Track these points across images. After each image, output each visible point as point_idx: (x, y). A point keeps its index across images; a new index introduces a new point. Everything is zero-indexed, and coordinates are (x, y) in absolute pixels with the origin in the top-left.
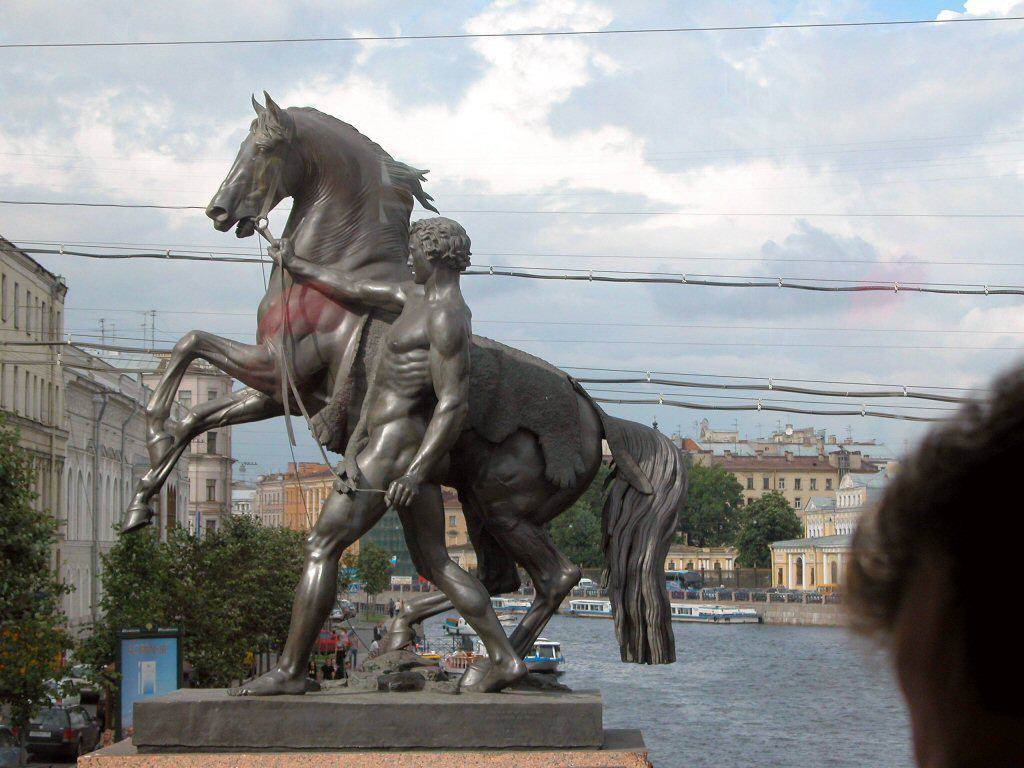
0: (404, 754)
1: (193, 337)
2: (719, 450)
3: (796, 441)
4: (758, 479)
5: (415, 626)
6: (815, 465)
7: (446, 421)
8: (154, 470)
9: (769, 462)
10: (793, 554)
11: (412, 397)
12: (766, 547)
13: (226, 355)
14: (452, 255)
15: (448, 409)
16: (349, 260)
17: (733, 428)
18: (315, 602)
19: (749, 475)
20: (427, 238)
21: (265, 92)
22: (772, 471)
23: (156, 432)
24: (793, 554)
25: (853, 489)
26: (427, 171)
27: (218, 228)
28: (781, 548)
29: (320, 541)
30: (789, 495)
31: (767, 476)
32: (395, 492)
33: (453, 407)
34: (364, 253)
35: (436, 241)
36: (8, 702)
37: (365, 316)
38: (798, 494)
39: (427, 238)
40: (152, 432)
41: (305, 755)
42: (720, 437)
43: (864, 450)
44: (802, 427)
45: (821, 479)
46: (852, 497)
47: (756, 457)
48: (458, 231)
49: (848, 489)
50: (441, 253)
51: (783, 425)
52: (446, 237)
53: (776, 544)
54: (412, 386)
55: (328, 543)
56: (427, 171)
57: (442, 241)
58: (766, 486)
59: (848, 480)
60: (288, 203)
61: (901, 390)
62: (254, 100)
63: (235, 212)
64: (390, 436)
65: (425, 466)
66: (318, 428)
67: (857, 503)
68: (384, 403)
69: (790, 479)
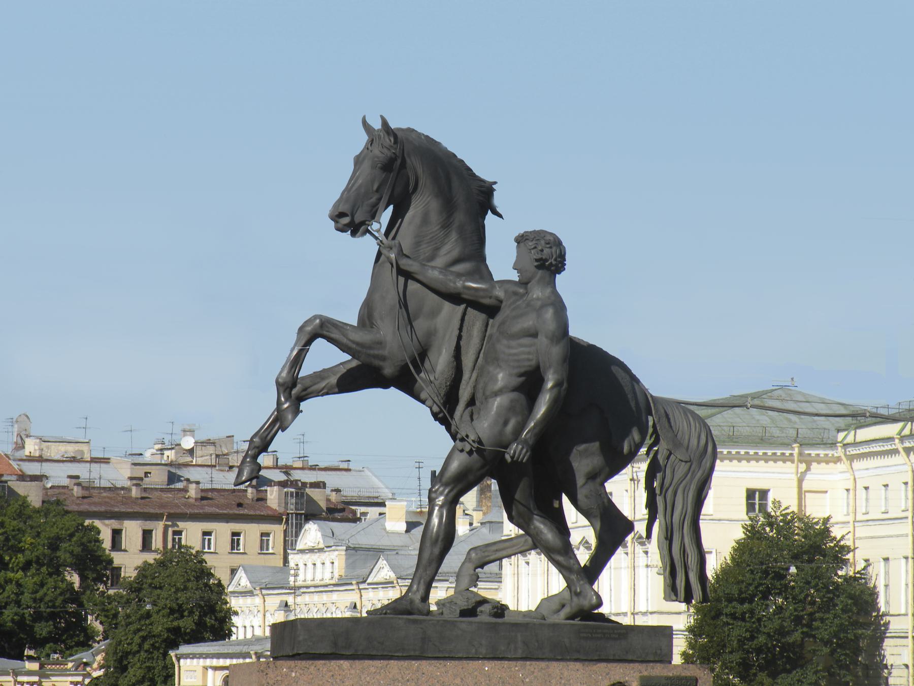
0: (519, 663)
1: (318, 321)
2: (58, 475)
3: (200, 461)
4: (132, 530)
5: (479, 570)
8: (652, 415)
9: (163, 499)
10: (216, 669)
13: (345, 335)
15: (552, 388)
16: (440, 261)
18: (440, 539)
19: (115, 524)
20: (535, 248)
21: (382, 117)
22: (157, 517)
24: (216, 669)
25: (321, 550)
26: (495, 183)
27: (338, 229)
28: (193, 656)
29: (444, 490)
30: (218, 563)
31: (149, 525)
32: (515, 452)
33: (558, 385)
34: (455, 253)
35: (542, 250)
36: (226, 603)
39: (535, 248)
41: (441, 662)
42: (56, 451)
43: (332, 480)
44: (212, 436)
45: (251, 532)
46: (319, 565)
47: (128, 490)
48: (558, 243)
49: (311, 550)
50: (546, 260)
51: (177, 429)
53: (184, 649)
55: (449, 492)
56: (495, 183)
57: (546, 251)
58: (146, 545)
59: (312, 534)
60: (391, 208)
62: (365, 123)
63: (350, 219)
65: (536, 431)
66: (779, 392)
67: (327, 576)
69: (222, 531)
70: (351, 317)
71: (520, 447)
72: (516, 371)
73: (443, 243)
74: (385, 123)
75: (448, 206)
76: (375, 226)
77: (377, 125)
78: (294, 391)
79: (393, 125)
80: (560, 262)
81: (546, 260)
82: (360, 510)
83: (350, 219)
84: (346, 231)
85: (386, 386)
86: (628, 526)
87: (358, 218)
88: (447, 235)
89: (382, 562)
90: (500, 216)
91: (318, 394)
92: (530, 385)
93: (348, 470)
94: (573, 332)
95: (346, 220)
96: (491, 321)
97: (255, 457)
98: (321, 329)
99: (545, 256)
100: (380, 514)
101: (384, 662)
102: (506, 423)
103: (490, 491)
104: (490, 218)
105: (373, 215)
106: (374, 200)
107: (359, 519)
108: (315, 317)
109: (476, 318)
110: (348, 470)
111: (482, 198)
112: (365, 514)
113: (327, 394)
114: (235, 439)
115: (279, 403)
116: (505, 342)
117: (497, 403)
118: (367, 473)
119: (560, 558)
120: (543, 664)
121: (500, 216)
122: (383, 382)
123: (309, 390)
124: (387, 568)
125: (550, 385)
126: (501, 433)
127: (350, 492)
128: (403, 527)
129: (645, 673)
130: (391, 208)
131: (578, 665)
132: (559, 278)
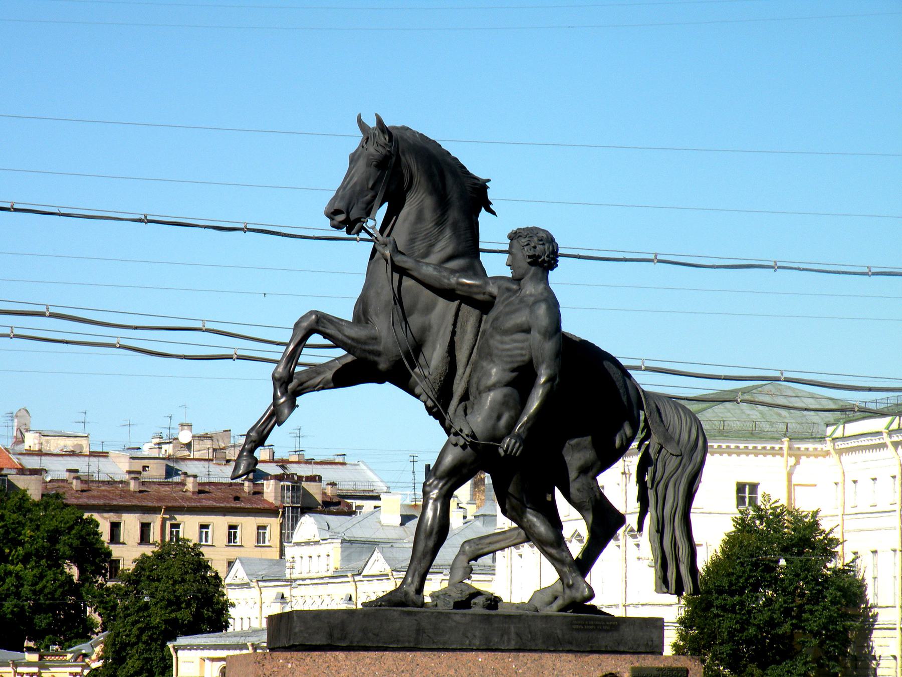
0: (513, 654)
2: (58, 469)
3: (197, 455)
4: (131, 523)
5: (473, 562)
6: (237, 498)
7: (546, 390)
8: (643, 410)
9: (160, 493)
11: (513, 370)
12: (163, 646)
14: (547, 259)
15: (545, 383)
16: (434, 258)
17: (78, 430)
18: (434, 532)
19: (113, 517)
20: (528, 244)
21: (377, 115)
22: (155, 510)
23: (283, 395)
25: (317, 543)
26: (489, 180)
27: (333, 226)
28: (191, 647)
29: (438, 484)
30: (216, 556)
31: (147, 518)
33: (550, 380)
34: (449, 250)
35: (535, 247)
37: (457, 302)
38: (233, 553)
39: (528, 244)
40: (279, 394)
41: (436, 653)
43: (328, 473)
47: (126, 483)
50: (539, 257)
51: (175, 424)
52: (543, 244)
53: (182, 641)
54: (513, 362)
55: (443, 486)
56: (489, 180)
57: (540, 248)
58: (144, 538)
60: (386, 205)
61: (778, 374)
63: (346, 217)
64: (493, 401)
68: (488, 374)
69: (219, 524)
70: (345, 311)
71: (513, 441)
72: (509, 366)
73: (437, 240)
74: (380, 122)
75: (442, 204)
76: (370, 223)
77: (372, 123)
78: (291, 386)
79: (388, 123)
80: (553, 259)
81: (539, 257)
82: (355, 503)
83: (346, 217)
84: (341, 228)
85: (381, 381)
86: (620, 520)
87: (354, 215)
88: (441, 232)
89: (377, 555)
90: (493, 213)
91: (314, 388)
92: (522, 379)
93: (344, 464)
94: (571, 326)
95: (341, 217)
96: (485, 317)
97: (252, 451)
98: (317, 324)
99: (539, 254)
100: (375, 507)
101: (379, 654)
102: (499, 418)
103: (484, 484)
104: (483, 215)
105: (368, 212)
106: (369, 197)
107: (355, 513)
108: (311, 313)
109: (470, 314)
110: (344, 464)
111: (476, 196)
112: (360, 507)
113: (323, 388)
114: (232, 433)
115: (275, 398)
116: (498, 337)
117: (490, 399)
118: (362, 466)
119: (553, 551)
120: (536, 655)
121: (493, 213)
122: (379, 379)
123: (306, 385)
124: (382, 560)
125: (543, 380)
126: (494, 427)
127: (345, 486)
128: (399, 520)
129: (637, 665)
130: (386, 205)
131: (571, 656)
132: (551, 274)
